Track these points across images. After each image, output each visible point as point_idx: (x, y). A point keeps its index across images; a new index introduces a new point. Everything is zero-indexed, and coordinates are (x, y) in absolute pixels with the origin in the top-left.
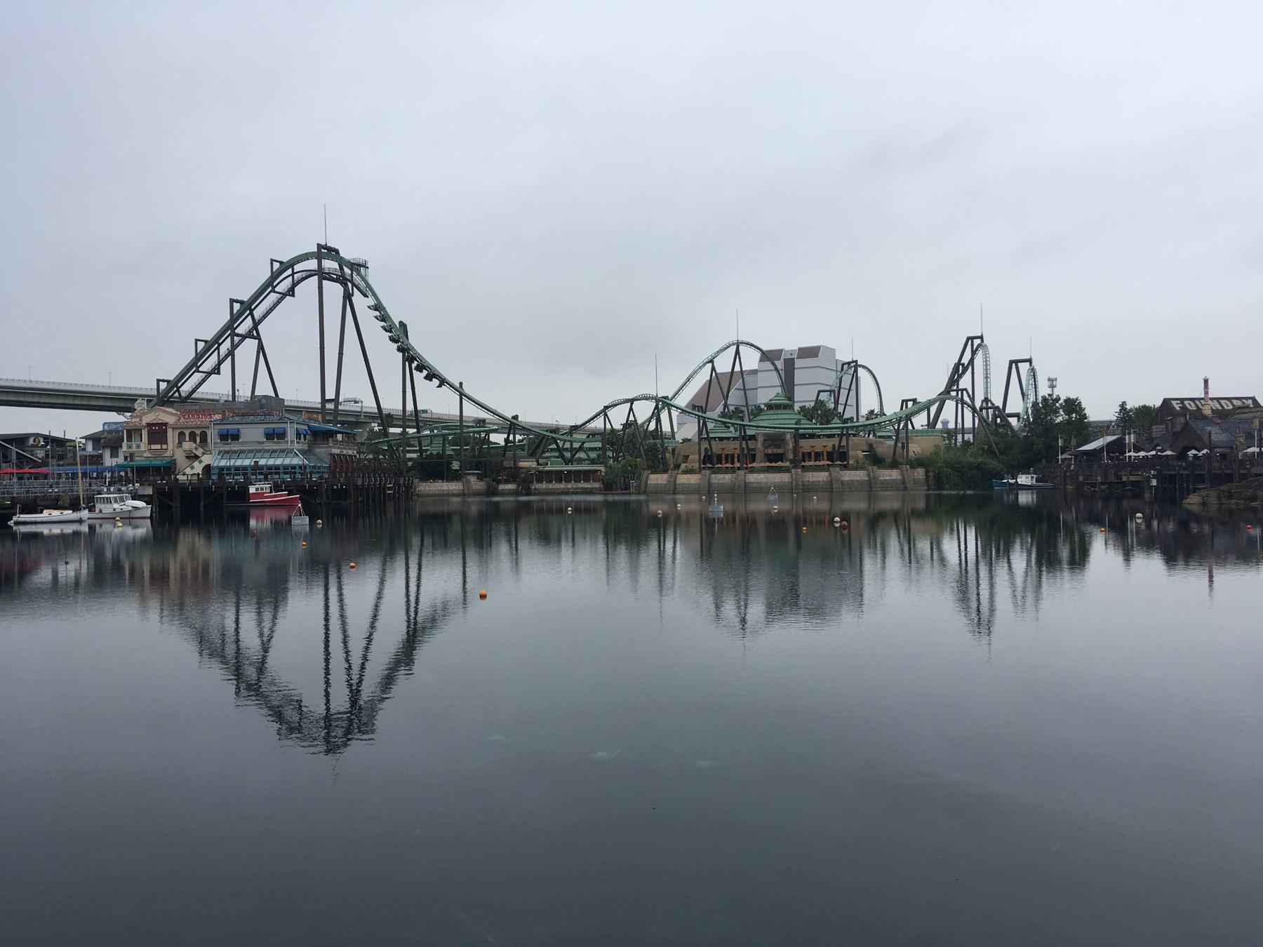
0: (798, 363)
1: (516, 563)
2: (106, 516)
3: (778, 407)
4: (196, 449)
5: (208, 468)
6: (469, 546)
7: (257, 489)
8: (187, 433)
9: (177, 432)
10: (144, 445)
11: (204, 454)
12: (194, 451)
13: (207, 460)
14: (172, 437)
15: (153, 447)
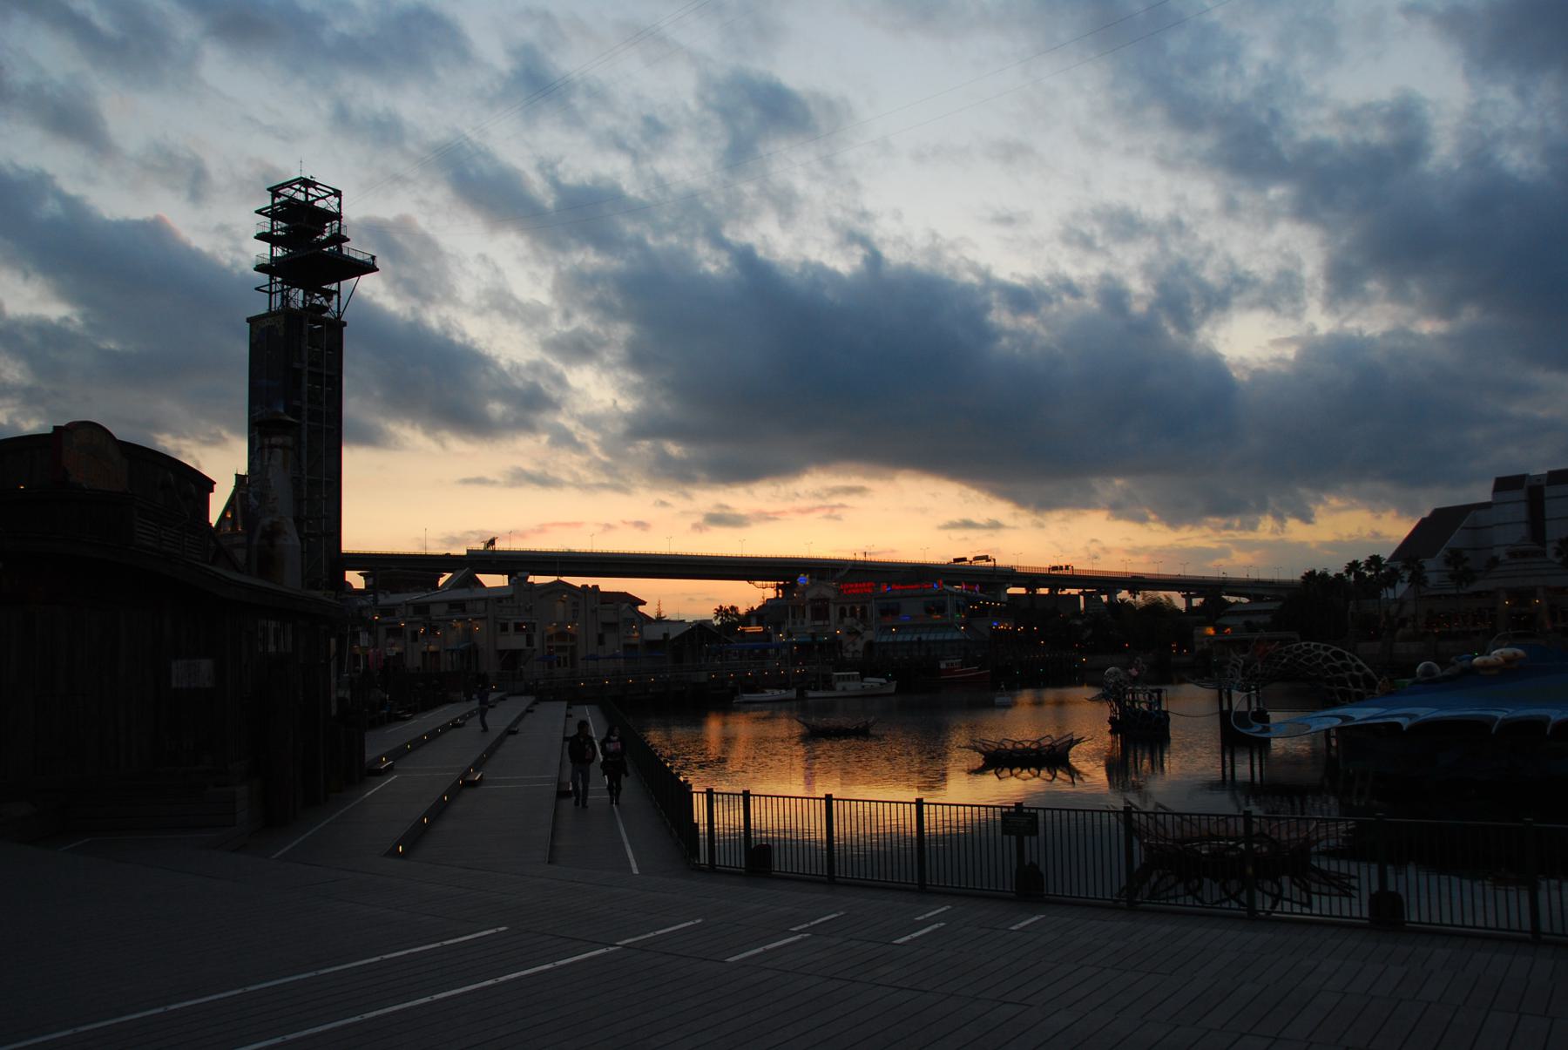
0: (1549, 492)
1: (466, 481)
2: (852, 694)
3: (1524, 554)
4: (857, 624)
5: (870, 645)
6: (371, 438)
7: (947, 665)
8: (848, 608)
9: (838, 607)
10: (807, 622)
11: (864, 629)
12: (855, 627)
13: (869, 635)
14: (834, 612)
15: (817, 623)
